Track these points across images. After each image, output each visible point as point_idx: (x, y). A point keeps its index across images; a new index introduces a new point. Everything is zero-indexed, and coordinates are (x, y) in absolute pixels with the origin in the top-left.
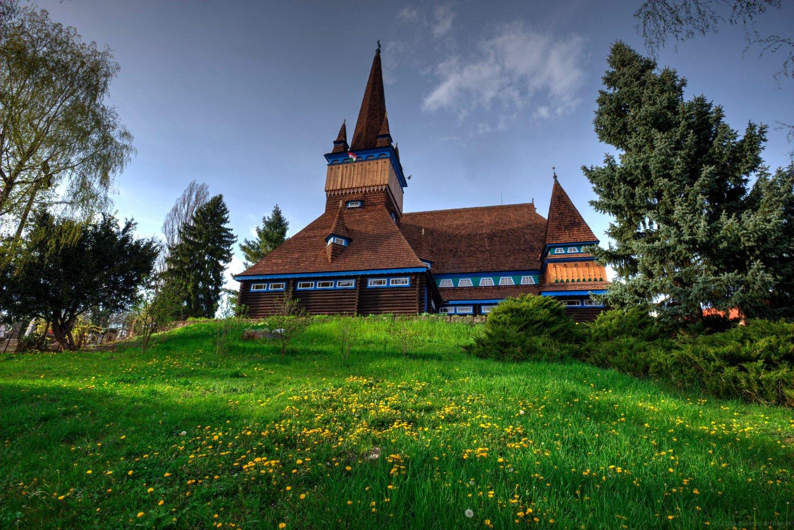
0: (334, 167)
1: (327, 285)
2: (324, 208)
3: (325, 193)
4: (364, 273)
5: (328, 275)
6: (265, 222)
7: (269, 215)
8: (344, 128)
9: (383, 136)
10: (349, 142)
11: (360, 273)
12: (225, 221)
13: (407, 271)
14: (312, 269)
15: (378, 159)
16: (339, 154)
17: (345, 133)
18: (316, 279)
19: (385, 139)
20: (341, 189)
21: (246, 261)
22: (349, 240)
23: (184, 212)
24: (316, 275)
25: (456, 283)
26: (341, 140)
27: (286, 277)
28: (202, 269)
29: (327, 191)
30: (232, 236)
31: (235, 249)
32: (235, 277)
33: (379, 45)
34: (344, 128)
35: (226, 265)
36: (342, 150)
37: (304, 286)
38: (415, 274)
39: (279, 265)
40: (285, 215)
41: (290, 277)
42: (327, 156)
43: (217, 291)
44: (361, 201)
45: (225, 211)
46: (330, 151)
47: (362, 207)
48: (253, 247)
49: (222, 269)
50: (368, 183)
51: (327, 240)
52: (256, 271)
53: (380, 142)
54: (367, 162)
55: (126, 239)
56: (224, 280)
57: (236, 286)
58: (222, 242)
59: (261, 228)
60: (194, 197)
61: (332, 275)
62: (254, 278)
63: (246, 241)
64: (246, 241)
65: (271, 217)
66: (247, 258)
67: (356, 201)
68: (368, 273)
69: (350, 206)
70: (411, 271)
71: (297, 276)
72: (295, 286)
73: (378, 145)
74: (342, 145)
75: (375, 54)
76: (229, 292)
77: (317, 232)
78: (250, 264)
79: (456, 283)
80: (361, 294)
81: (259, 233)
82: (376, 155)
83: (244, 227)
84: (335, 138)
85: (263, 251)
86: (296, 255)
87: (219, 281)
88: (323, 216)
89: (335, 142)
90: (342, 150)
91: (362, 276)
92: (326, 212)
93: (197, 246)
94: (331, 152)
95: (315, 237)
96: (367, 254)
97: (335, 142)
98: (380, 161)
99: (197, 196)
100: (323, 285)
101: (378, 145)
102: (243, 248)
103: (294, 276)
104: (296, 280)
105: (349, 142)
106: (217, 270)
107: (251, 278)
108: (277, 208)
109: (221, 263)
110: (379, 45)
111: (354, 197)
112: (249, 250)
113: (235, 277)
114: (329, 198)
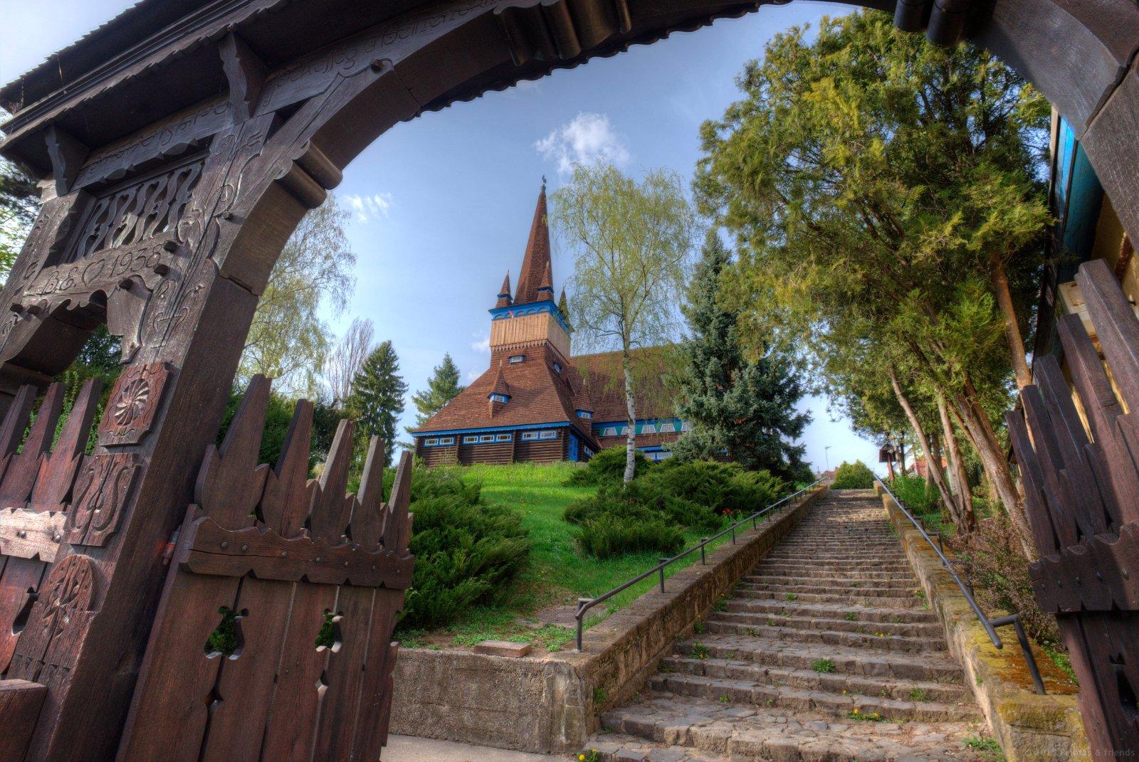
0: (498, 322)
1: (488, 439)
6: (436, 371)
7: (440, 363)
8: (507, 280)
9: (545, 289)
10: (513, 294)
12: (395, 369)
14: (475, 426)
15: (538, 313)
16: (507, 305)
19: (546, 292)
20: (504, 345)
21: (418, 413)
22: (509, 397)
23: (348, 354)
25: (619, 431)
26: (505, 295)
28: (374, 421)
30: (403, 385)
31: (407, 399)
32: (410, 431)
33: (545, 181)
34: (507, 280)
35: (399, 416)
36: (505, 305)
38: (561, 428)
39: (451, 422)
40: (458, 363)
42: (492, 311)
43: (391, 444)
45: (395, 358)
46: (494, 306)
48: (425, 398)
49: (394, 420)
50: (529, 337)
51: (489, 397)
52: (432, 427)
53: (542, 296)
56: (397, 433)
57: (410, 440)
58: (393, 391)
59: (433, 378)
60: (358, 336)
63: (418, 393)
64: (418, 393)
65: (442, 366)
66: (420, 410)
69: (512, 360)
70: (557, 425)
72: (461, 441)
73: (539, 298)
74: (505, 298)
75: (539, 192)
76: (404, 445)
77: (482, 389)
78: (423, 415)
79: (619, 431)
80: (516, 446)
81: (431, 384)
83: (416, 375)
85: (435, 402)
86: (463, 412)
87: (391, 434)
88: (489, 371)
91: (517, 431)
93: (369, 398)
95: (480, 394)
96: (521, 410)
98: (540, 315)
99: (361, 336)
100: (486, 439)
101: (539, 298)
102: (416, 400)
104: (463, 435)
105: (513, 294)
106: (390, 421)
108: (448, 356)
109: (393, 414)
110: (545, 181)
111: (516, 352)
113: (410, 431)
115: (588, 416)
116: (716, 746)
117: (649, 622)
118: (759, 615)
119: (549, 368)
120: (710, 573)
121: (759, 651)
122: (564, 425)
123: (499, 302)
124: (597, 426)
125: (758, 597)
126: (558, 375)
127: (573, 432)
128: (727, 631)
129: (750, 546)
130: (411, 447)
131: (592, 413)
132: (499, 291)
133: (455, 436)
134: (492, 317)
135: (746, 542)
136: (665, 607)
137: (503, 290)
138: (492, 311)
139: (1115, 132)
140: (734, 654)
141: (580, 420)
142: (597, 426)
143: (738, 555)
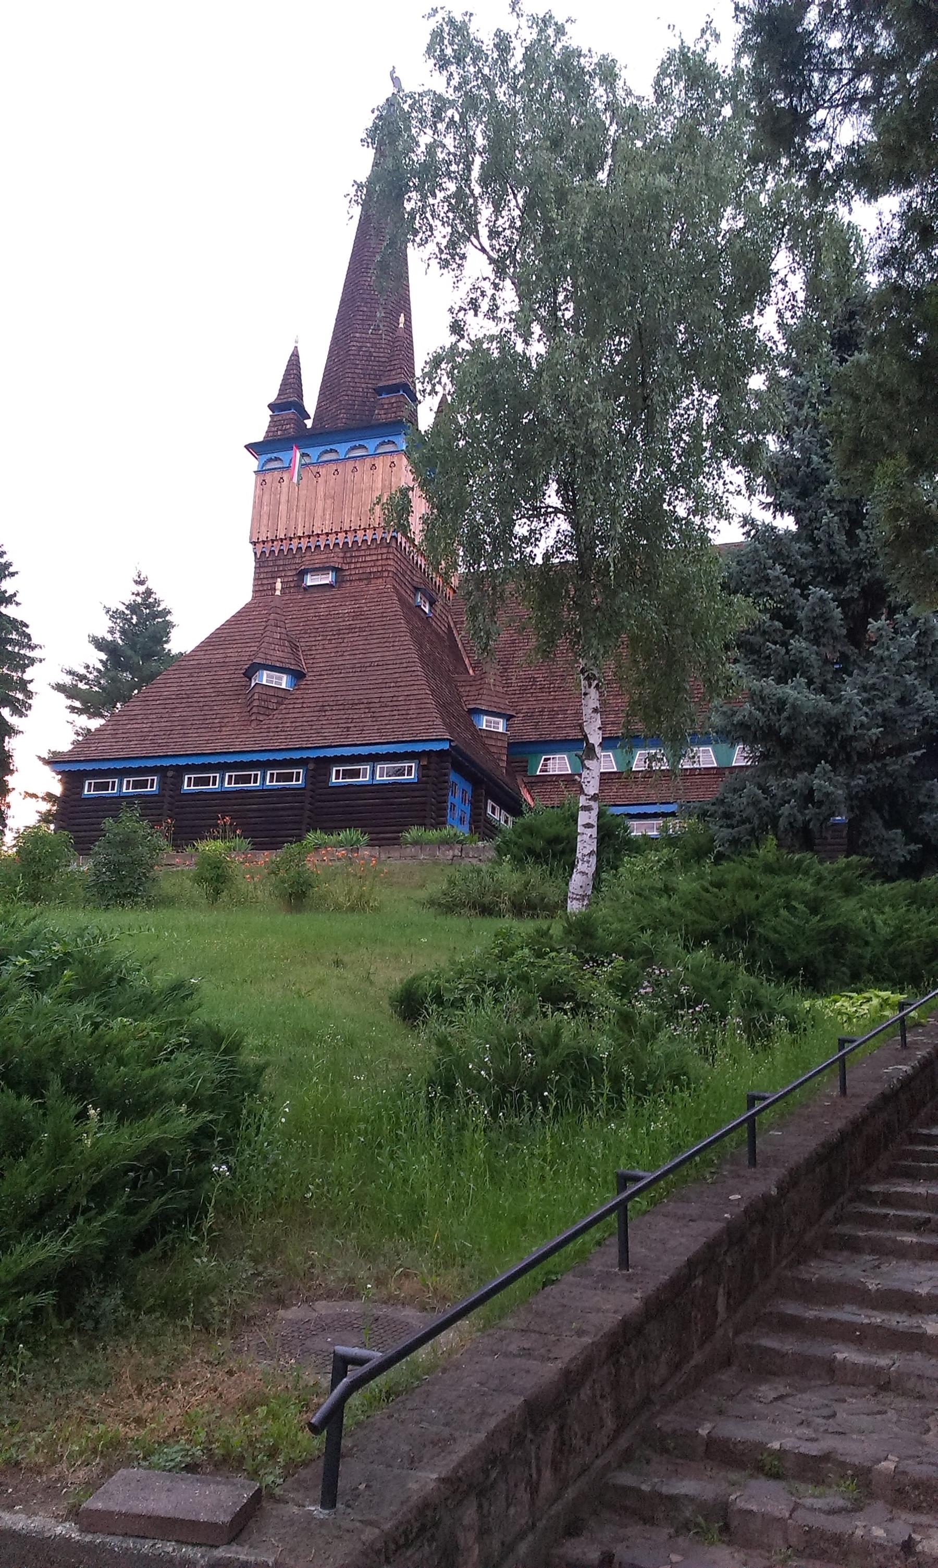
0: (268, 478)
2: (250, 588)
3: (251, 546)
4: (321, 753)
5: (105, 766)
10: (310, 403)
11: (313, 754)
13: (409, 748)
16: (288, 434)
17: (298, 377)
18: (122, 773)
21: (69, 702)
22: (297, 675)
24: (222, 759)
27: (305, 755)
29: (254, 543)
31: (41, 677)
36: (291, 428)
37: (198, 782)
41: (166, 763)
44: (336, 570)
46: (259, 436)
47: (340, 581)
54: (350, 465)
55: (702, 62)
61: (255, 757)
62: (89, 767)
67: (323, 570)
68: (330, 753)
69: (310, 581)
70: (419, 748)
71: (182, 762)
74: (290, 413)
82: (371, 444)
84: (272, 396)
89: (271, 407)
90: (291, 428)
92: (254, 598)
94: (261, 439)
97: (271, 407)
103: (174, 762)
104: (181, 770)
105: (310, 403)
107: (82, 767)
112: (84, 696)
114: (261, 561)
115: (500, 726)
116: (815, 1543)
117: (571, 1380)
118: (899, 1321)
119: (401, 600)
120: (766, 1198)
121: (888, 1465)
122: (436, 747)
123: (273, 422)
124: (522, 751)
125: (901, 1252)
126: (426, 619)
127: (459, 768)
128: (852, 1246)
129: (887, 1099)
130: (49, 797)
131: (509, 718)
132: (272, 395)
133: (159, 771)
134: (253, 463)
135: (879, 1088)
136: (625, 1323)
137: (282, 391)
138: (253, 448)
139: (203, 951)
140: (812, 1469)
141: (479, 735)
142: (522, 751)
143: (856, 1127)
